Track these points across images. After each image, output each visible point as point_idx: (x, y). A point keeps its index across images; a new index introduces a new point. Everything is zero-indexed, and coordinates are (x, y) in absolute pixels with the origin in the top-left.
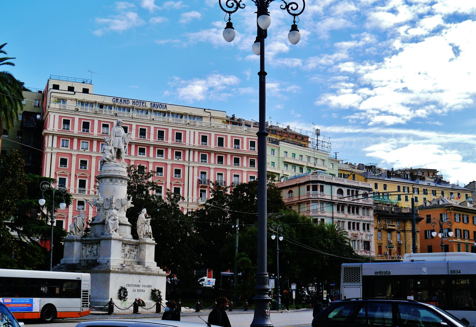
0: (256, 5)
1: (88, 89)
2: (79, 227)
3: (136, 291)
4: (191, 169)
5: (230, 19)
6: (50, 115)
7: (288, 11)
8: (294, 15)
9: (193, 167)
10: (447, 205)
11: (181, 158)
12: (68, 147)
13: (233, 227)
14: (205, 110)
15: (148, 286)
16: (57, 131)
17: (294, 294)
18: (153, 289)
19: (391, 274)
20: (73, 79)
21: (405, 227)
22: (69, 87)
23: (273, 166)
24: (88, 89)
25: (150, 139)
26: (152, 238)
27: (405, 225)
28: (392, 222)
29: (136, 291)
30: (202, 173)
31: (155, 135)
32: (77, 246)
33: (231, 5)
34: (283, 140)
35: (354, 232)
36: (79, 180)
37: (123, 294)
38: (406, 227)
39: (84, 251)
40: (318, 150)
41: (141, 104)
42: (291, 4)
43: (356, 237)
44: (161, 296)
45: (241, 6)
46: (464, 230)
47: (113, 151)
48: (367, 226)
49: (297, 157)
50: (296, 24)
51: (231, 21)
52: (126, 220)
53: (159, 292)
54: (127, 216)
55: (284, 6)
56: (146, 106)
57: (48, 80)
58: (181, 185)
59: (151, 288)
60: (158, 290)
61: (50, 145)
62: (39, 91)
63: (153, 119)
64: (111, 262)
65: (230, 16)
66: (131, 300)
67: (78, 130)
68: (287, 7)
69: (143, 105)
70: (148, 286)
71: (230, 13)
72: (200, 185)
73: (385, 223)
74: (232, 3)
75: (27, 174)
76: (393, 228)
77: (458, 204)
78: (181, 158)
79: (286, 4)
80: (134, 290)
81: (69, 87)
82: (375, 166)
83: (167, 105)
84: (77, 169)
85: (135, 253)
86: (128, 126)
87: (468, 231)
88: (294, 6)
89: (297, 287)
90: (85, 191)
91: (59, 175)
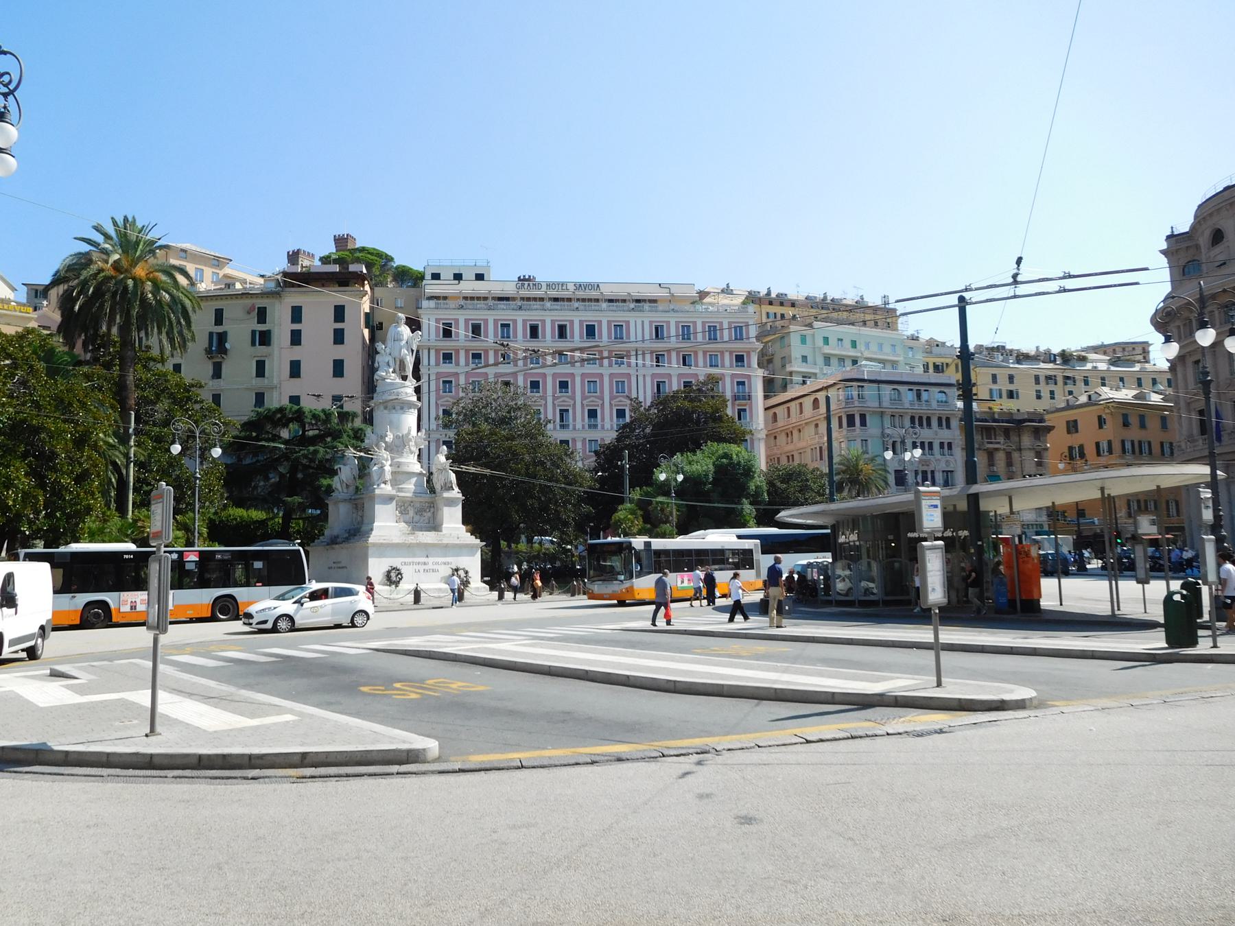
1: (439, 274)
4: (641, 379)
9: (644, 376)
10: (1103, 400)
13: (619, 463)
14: (660, 285)
15: (445, 564)
18: (454, 567)
21: (1020, 442)
23: (804, 364)
24: (439, 274)
26: (456, 489)
27: (1020, 440)
29: (422, 571)
30: (739, 383)
37: (393, 577)
43: (928, 465)
46: (1140, 442)
47: (392, 363)
49: (832, 341)
58: (570, 406)
60: (464, 569)
66: (407, 586)
67: (523, 338)
70: (445, 564)
72: (737, 402)
73: (982, 439)
77: (1130, 397)
84: (554, 392)
85: (429, 514)
86: (665, 324)
87: (1149, 443)
91: (587, 405)
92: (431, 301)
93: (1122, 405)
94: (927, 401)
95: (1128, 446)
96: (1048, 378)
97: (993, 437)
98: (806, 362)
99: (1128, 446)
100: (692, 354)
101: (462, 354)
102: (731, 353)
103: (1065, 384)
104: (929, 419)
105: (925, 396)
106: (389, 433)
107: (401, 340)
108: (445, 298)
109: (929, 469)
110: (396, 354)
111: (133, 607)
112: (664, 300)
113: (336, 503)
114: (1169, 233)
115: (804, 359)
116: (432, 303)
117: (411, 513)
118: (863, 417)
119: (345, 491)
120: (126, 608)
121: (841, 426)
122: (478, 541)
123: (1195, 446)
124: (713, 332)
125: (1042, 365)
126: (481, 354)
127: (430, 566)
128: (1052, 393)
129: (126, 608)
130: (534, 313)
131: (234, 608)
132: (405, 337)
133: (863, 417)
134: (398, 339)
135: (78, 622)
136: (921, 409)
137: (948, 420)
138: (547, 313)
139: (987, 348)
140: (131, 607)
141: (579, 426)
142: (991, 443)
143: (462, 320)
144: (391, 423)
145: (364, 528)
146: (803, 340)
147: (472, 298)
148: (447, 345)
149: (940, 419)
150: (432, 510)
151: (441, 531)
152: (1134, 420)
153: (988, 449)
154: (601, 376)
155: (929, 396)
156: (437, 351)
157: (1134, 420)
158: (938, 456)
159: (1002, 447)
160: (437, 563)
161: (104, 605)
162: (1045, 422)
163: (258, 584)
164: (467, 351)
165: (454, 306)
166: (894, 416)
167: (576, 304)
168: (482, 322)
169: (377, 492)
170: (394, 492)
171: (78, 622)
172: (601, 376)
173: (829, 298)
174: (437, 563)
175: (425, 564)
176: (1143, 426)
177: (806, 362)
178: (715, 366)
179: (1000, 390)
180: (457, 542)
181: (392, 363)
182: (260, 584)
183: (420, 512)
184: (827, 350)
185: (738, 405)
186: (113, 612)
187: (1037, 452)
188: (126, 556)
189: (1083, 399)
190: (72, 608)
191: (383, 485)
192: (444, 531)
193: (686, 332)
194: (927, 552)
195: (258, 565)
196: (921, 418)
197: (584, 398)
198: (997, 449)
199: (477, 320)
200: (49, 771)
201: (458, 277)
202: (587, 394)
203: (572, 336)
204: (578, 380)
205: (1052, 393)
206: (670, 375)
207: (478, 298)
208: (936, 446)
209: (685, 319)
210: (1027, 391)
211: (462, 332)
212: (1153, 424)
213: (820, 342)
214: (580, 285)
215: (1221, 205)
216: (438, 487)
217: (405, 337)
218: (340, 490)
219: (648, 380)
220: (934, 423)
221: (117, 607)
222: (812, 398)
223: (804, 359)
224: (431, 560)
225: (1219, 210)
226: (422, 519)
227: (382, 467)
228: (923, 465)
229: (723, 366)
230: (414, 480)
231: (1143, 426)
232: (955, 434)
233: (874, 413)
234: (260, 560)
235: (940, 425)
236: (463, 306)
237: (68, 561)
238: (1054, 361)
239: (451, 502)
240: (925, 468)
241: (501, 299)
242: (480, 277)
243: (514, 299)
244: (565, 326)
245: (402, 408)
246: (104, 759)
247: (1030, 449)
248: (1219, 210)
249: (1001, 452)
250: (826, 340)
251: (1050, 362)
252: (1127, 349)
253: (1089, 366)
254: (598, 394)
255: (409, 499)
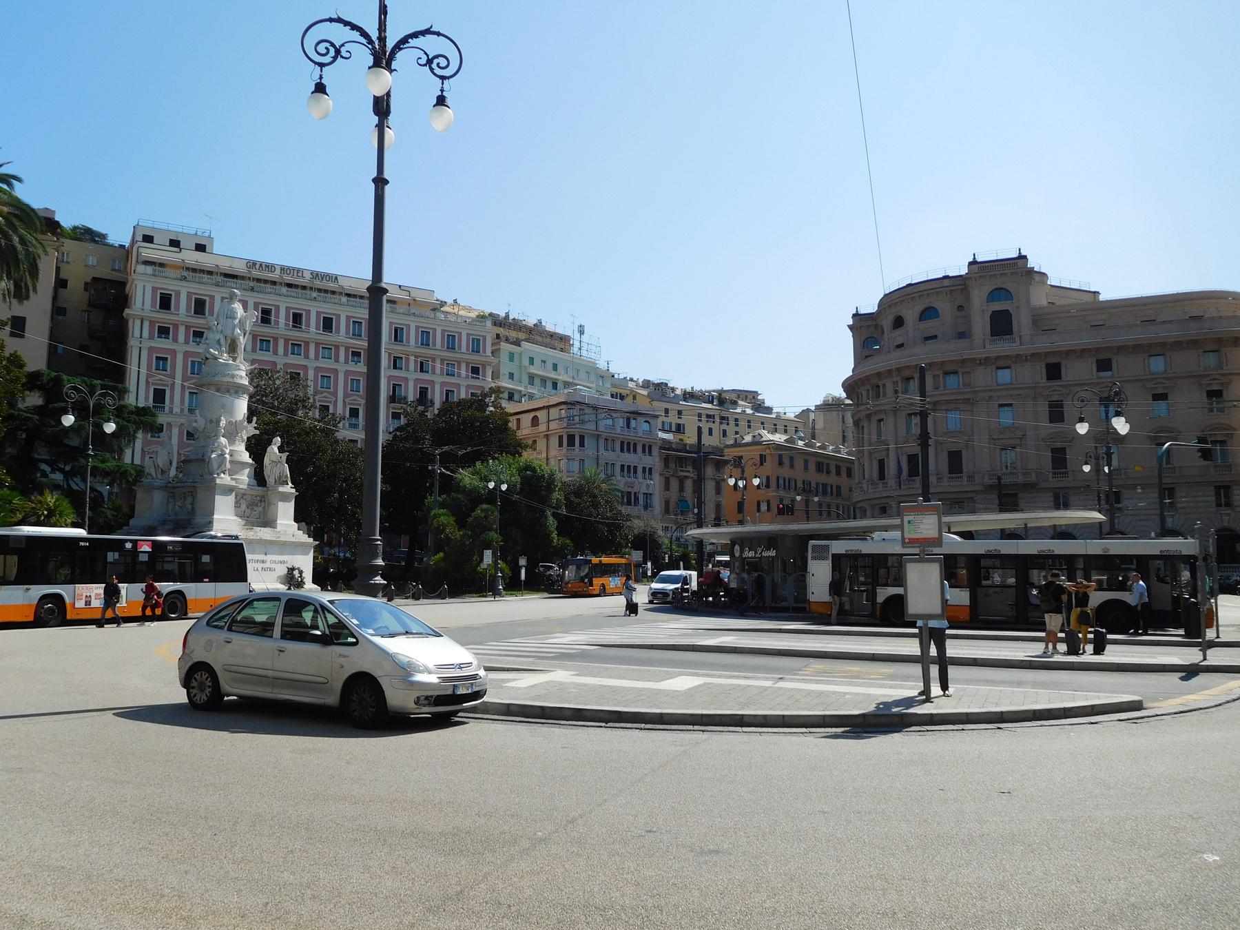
0: (372, 54)
2: (161, 465)
3: (260, 569)
5: (321, 77)
6: (136, 285)
7: (432, 70)
8: (443, 78)
10: (766, 441)
11: (360, 362)
12: (300, 355)
13: (430, 468)
14: (400, 286)
15: (281, 562)
16: (184, 316)
17: (523, 572)
18: (290, 567)
19: (863, 553)
20: (165, 224)
22: (196, 244)
23: (511, 381)
25: (179, 311)
26: (290, 484)
28: (686, 466)
29: (260, 569)
31: (287, 319)
32: (158, 497)
33: (324, 51)
34: (527, 340)
35: (629, 480)
36: (154, 389)
38: (706, 474)
39: (171, 505)
40: (581, 356)
41: (296, 272)
42: (437, 57)
44: (304, 578)
45: (344, 54)
46: (789, 479)
47: (223, 341)
48: (648, 472)
49: (537, 362)
50: (444, 94)
51: (323, 81)
52: (246, 457)
53: (301, 572)
54: (246, 449)
55: (424, 61)
56: (302, 277)
57: (134, 227)
59: (286, 565)
60: (298, 569)
61: (137, 333)
62: (120, 245)
63: (315, 298)
64: (214, 524)
65: (321, 71)
67: (152, 306)
68: (430, 62)
69: (299, 274)
70: (281, 562)
71: (322, 65)
74: (327, 48)
75: (62, 380)
76: (687, 474)
77: (782, 440)
78: (360, 362)
79: (428, 56)
80: (256, 569)
81: (196, 244)
82: (666, 384)
83: (338, 277)
85: (261, 509)
87: (796, 480)
88: (443, 62)
89: (528, 561)
90: (164, 407)
92: (148, 267)
93: (778, 447)
94: (635, 429)
95: (781, 482)
96: (708, 416)
97: (684, 466)
98: (513, 379)
99: (781, 482)
100: (303, 344)
101: (182, 330)
102: (468, 364)
103: (721, 423)
104: (635, 445)
105: (633, 423)
106: (222, 418)
107: (235, 319)
108: (162, 265)
109: (633, 491)
110: (228, 332)
111: (88, 603)
112: (402, 301)
113: (149, 489)
114: (855, 312)
115: (511, 376)
116: (149, 269)
117: (244, 507)
118: (582, 438)
119: (159, 477)
120: (80, 604)
121: (561, 445)
122: (311, 540)
123: (875, 488)
124: (451, 342)
125: (704, 405)
126: (360, 353)
127: (268, 565)
128: (710, 430)
129: (80, 604)
130: (267, 296)
131: (181, 603)
132: (239, 316)
133: (582, 438)
134: (231, 316)
135: (31, 619)
136: (629, 436)
137: (650, 447)
138: (282, 299)
139: (653, 384)
140: (86, 602)
141: (177, 410)
142: (683, 471)
143: (183, 293)
144: (223, 406)
145: (198, 520)
146: (511, 357)
147: (194, 270)
148: (164, 317)
149: (644, 446)
150: (263, 504)
151: (276, 528)
152: (786, 461)
153: (680, 476)
154: (174, 352)
155: (636, 425)
156: (152, 323)
157: (786, 461)
158: (641, 480)
159: (692, 475)
160: (274, 562)
161: (58, 599)
162: (724, 456)
163: (205, 580)
164: (187, 328)
165: (174, 276)
166: (607, 440)
167: (315, 294)
168: (273, 308)
169: (218, 481)
170: (233, 483)
171: (31, 619)
172: (174, 352)
173: (511, 317)
174: (274, 562)
175: (263, 562)
176: (792, 466)
177: (513, 379)
178: (451, 375)
179: (671, 423)
180: (293, 540)
181: (223, 341)
182: (207, 580)
183: (251, 505)
184: (533, 370)
185: (393, 408)
186: (68, 607)
187: (666, 478)
188: (82, 544)
189: (748, 439)
190: (27, 602)
191: (222, 475)
192: (279, 528)
193: (425, 337)
194: (140, 554)
195: (206, 559)
196: (629, 444)
197: (346, 396)
198: (686, 477)
199: (201, 295)
200: (1125, 718)
201: (175, 243)
202: (349, 392)
203: (177, 308)
204: (341, 377)
205: (710, 430)
206: (407, 379)
207: (202, 271)
208: (640, 470)
209: (425, 324)
210: (690, 422)
211: (282, 320)
212: (799, 464)
213: (526, 362)
214: (317, 275)
215: (904, 298)
216: (270, 480)
217: (239, 316)
218: (155, 476)
219: (145, 354)
220: (639, 449)
221: (72, 602)
222: (532, 415)
223: (511, 376)
224: (269, 558)
225: (902, 301)
226: (254, 513)
227: (222, 455)
228: (628, 487)
229: (434, 373)
230: (247, 471)
231: (792, 466)
232: (654, 461)
233: (592, 435)
234: (207, 554)
235: (644, 451)
236: (186, 278)
237: (24, 546)
238: (712, 402)
239: (285, 497)
240: (630, 489)
241: (227, 275)
242: (201, 248)
243: (243, 278)
244: (301, 315)
245: (236, 392)
246: (965, 718)
247: (712, 479)
248: (902, 301)
249: (689, 479)
250: (532, 360)
251: (709, 403)
252: (741, 396)
253: (739, 410)
254: (332, 390)
255: (243, 491)
